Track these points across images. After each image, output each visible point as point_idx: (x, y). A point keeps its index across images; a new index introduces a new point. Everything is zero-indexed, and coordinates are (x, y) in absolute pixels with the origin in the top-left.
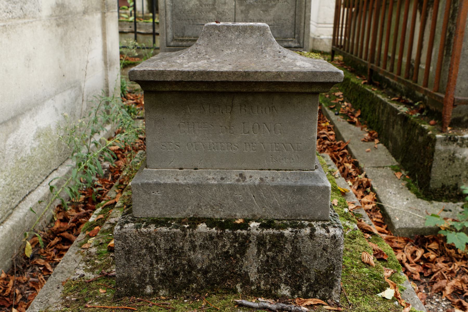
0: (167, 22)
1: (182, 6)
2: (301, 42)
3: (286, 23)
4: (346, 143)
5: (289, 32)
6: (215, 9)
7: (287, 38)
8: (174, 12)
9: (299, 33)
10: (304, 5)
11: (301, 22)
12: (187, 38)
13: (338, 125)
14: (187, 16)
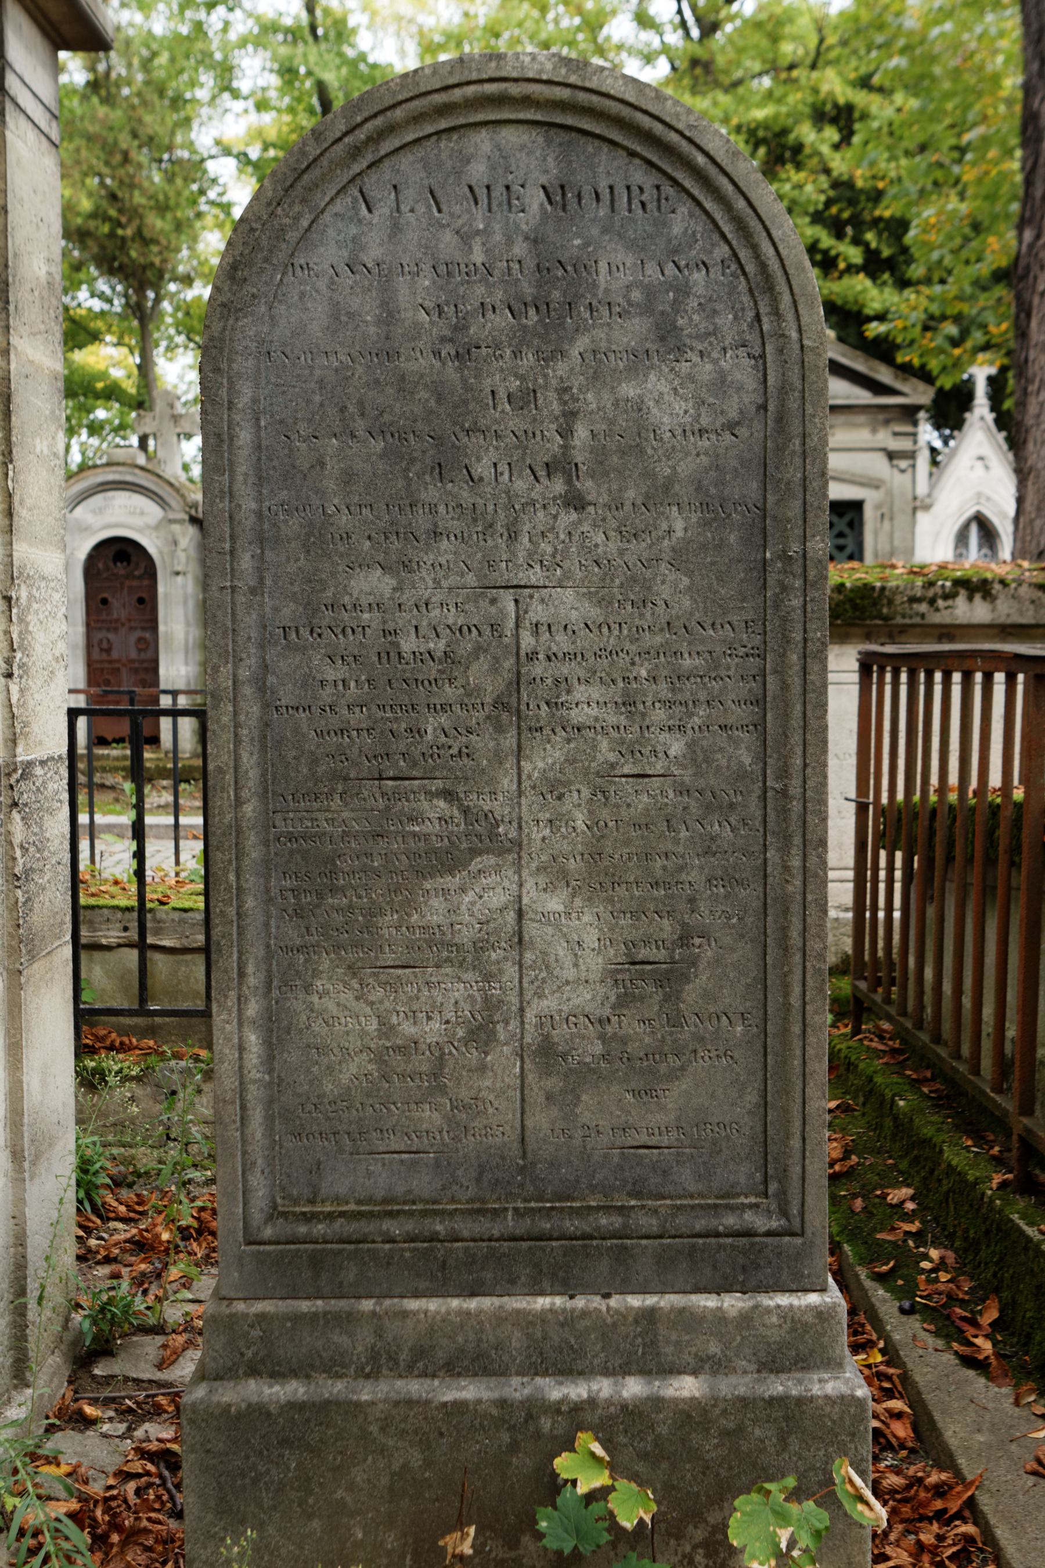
0: (250, 1149)
1: (311, 1082)
2: (795, 1211)
3: (728, 1137)
4: (968, 1485)
5: (744, 1173)
6: (442, 1089)
7: (738, 1195)
8: (276, 1107)
9: (783, 1176)
10: (798, 1070)
11: (788, 1136)
12: (328, 1209)
13: (922, 1376)
14: (328, 1119)
